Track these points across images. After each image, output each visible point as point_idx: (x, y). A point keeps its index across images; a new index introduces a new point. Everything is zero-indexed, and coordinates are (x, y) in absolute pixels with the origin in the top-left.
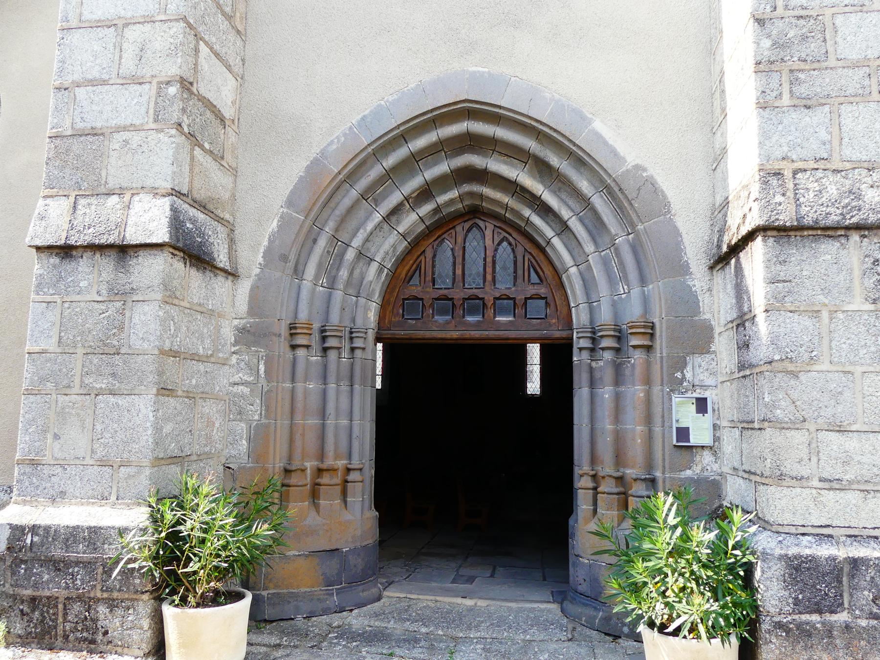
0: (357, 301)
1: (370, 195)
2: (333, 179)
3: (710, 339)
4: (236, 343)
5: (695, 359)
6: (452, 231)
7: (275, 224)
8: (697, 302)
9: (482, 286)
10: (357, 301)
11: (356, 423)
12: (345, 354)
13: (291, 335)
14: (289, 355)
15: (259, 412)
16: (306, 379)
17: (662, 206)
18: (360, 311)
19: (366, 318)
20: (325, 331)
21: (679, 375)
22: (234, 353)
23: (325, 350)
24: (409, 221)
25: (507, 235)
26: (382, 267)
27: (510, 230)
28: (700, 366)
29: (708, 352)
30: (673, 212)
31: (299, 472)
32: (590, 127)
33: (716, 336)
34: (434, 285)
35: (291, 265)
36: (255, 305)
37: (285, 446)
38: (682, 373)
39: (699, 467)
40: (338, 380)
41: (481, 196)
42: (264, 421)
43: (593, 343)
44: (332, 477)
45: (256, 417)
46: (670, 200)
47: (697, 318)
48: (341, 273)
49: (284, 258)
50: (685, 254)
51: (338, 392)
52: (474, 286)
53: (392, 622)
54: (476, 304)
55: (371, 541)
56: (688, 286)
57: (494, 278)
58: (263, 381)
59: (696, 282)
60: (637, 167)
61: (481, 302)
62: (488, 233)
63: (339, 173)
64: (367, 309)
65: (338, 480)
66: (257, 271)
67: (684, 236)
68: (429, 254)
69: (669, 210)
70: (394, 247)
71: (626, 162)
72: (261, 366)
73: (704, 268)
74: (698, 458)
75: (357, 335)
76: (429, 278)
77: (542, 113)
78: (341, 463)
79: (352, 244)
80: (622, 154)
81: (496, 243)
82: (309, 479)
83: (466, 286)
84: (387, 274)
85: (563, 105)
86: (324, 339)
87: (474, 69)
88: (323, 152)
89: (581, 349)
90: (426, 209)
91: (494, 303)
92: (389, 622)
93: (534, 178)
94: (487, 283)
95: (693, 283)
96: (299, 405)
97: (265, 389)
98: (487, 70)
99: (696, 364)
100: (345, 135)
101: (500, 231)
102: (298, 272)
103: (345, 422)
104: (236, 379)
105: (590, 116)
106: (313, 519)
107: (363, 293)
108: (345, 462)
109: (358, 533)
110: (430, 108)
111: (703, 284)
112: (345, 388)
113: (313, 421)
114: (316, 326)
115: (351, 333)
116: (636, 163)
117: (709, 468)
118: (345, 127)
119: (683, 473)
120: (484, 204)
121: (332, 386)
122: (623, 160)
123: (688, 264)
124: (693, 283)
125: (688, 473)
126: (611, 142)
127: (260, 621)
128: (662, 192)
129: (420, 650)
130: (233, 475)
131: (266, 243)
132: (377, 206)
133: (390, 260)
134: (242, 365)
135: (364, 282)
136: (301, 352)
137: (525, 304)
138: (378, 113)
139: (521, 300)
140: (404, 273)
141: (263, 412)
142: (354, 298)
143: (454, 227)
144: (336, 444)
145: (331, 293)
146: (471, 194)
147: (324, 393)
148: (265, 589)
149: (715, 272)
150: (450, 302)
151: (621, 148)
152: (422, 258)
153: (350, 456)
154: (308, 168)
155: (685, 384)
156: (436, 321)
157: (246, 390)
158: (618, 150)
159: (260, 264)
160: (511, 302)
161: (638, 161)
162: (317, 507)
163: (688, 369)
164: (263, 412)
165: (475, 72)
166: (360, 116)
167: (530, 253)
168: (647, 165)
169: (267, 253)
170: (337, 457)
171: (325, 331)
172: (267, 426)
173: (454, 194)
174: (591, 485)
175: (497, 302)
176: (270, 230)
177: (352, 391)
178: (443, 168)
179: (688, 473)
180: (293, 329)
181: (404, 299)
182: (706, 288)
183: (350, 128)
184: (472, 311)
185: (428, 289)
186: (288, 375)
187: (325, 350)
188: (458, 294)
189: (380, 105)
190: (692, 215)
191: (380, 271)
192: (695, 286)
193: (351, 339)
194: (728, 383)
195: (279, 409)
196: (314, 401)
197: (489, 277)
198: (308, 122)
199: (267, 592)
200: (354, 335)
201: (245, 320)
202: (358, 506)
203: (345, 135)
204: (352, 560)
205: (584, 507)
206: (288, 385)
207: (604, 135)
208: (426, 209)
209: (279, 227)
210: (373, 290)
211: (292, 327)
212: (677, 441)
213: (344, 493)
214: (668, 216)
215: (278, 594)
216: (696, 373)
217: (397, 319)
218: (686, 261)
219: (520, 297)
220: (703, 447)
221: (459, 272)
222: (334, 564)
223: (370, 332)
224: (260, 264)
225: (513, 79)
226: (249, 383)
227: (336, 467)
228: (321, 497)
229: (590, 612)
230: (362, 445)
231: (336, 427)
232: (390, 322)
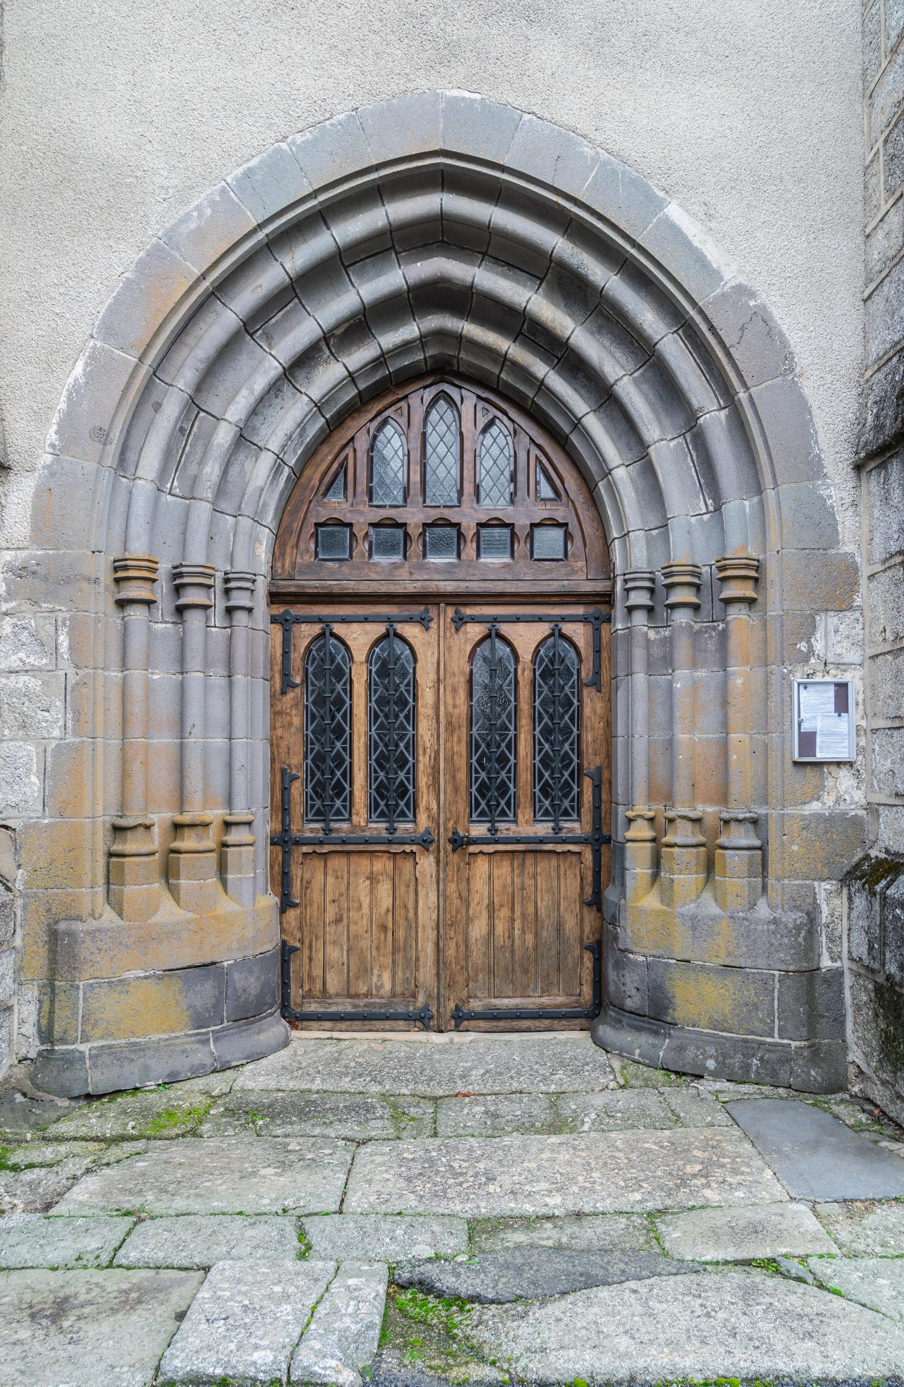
0: (236, 523)
1: (256, 323)
2: (192, 288)
3: (852, 586)
4: (10, 595)
5: (830, 620)
6: (403, 404)
7: (79, 369)
8: (834, 525)
9: (456, 503)
10: (236, 523)
11: (240, 743)
12: (217, 617)
13: (117, 581)
14: (114, 618)
15: (61, 723)
16: (148, 665)
17: (783, 361)
18: (242, 540)
19: (252, 556)
20: (180, 575)
21: (803, 646)
22: (6, 614)
23: (181, 610)
24: (328, 375)
25: (499, 414)
26: (279, 462)
27: (504, 406)
28: (836, 632)
29: (850, 608)
30: (798, 370)
31: (141, 830)
32: (661, 215)
33: (863, 581)
34: (371, 500)
35: (113, 449)
36: (45, 524)
37: (113, 787)
38: (809, 642)
39: (833, 797)
40: (207, 665)
41: (459, 339)
42: (70, 739)
43: (651, 598)
44: (200, 838)
45: (56, 733)
46: (793, 349)
47: (833, 551)
48: (207, 469)
49: (102, 436)
50: (816, 442)
51: (206, 688)
52: (442, 502)
53: (318, 1081)
54: (444, 532)
55: (269, 947)
56: (821, 497)
57: (477, 488)
58: (66, 666)
59: (833, 491)
60: (740, 290)
61: (453, 532)
62: (467, 408)
63: (203, 276)
64: (254, 540)
65: (210, 841)
66: (48, 459)
67: (815, 412)
68: (362, 443)
69: (791, 366)
70: (302, 426)
71: (721, 279)
72: (62, 638)
73: (845, 469)
74: (829, 782)
75: (239, 584)
76: (362, 487)
77: (578, 183)
78: (215, 814)
79: (228, 416)
80: (715, 266)
81: (480, 426)
82: (156, 843)
83: (428, 503)
84: (289, 478)
85: (615, 172)
86: (178, 589)
87: (455, 93)
88: (170, 236)
89: (630, 609)
90: (359, 356)
91: (477, 534)
92: (313, 1081)
93: (557, 306)
94: (464, 498)
95: (827, 492)
96: (137, 710)
97: (72, 679)
98: (477, 96)
99: (831, 628)
100: (212, 203)
101: (487, 406)
102: (124, 461)
103: (219, 741)
104: (14, 662)
105: (662, 194)
106: (168, 912)
107: (247, 509)
108: (220, 811)
109: (249, 933)
110: (374, 162)
111: (844, 494)
112: (218, 680)
113: (164, 740)
114: (164, 568)
115: (227, 581)
116: (738, 281)
117: (847, 797)
118: (211, 190)
119: (807, 807)
120: (462, 355)
121: (195, 677)
122: (715, 275)
123: (820, 460)
124: (827, 492)
125: (815, 806)
126: (696, 243)
127: (77, 1098)
128: (781, 334)
129: (379, 1123)
130: (14, 841)
131: (62, 406)
132: (270, 346)
133: (295, 451)
134: (24, 636)
135: (250, 490)
136: (137, 614)
137: (530, 536)
138: (276, 164)
139: (523, 527)
140: (318, 476)
141: (70, 724)
142: (231, 520)
143: (406, 397)
144: (205, 779)
145: (189, 506)
146: (440, 335)
147: (182, 691)
148: (85, 1039)
149: (864, 476)
150: (400, 532)
151: (713, 254)
152: (349, 451)
153: (229, 802)
154: (143, 266)
155: (813, 661)
156: (375, 564)
157: (34, 683)
158: (709, 257)
159: (52, 446)
160: (506, 531)
161: (742, 280)
162: (174, 891)
163: (818, 635)
164: (70, 724)
165: (456, 99)
166: (240, 170)
167: (539, 446)
168: (756, 285)
169: (67, 425)
170: (206, 804)
171: (180, 575)
172: (77, 749)
173: (410, 331)
174: (649, 834)
175: (483, 531)
176: (70, 380)
177: (231, 685)
178: (393, 278)
179: (815, 806)
180: (121, 572)
181: (317, 525)
182: (848, 500)
183: (223, 191)
184: (439, 547)
185: (361, 507)
186: (114, 656)
187: (181, 610)
188: (414, 516)
189: (279, 151)
190: (829, 377)
191: (277, 471)
192: (830, 497)
193: (227, 592)
194: (889, 657)
195: (100, 716)
196: (165, 704)
197: (468, 488)
198: (139, 174)
199: (89, 1045)
200: (232, 585)
201: (26, 553)
202: (247, 888)
203: (212, 203)
204: (239, 979)
205: (638, 870)
206: (115, 674)
207: (684, 229)
208: (359, 356)
209: (86, 374)
210: (265, 505)
211: (119, 566)
212: (800, 755)
213: (222, 868)
214: (790, 378)
215: (110, 1047)
216: (830, 643)
217: (306, 558)
218: (818, 455)
219: (522, 522)
220: (838, 764)
221: (416, 478)
222: (204, 992)
223: (260, 579)
224: (52, 446)
225: (526, 117)
226: (40, 670)
227: (207, 819)
228: (183, 872)
229: (645, 1039)
230: (250, 781)
231: (205, 748)
232: (293, 565)
